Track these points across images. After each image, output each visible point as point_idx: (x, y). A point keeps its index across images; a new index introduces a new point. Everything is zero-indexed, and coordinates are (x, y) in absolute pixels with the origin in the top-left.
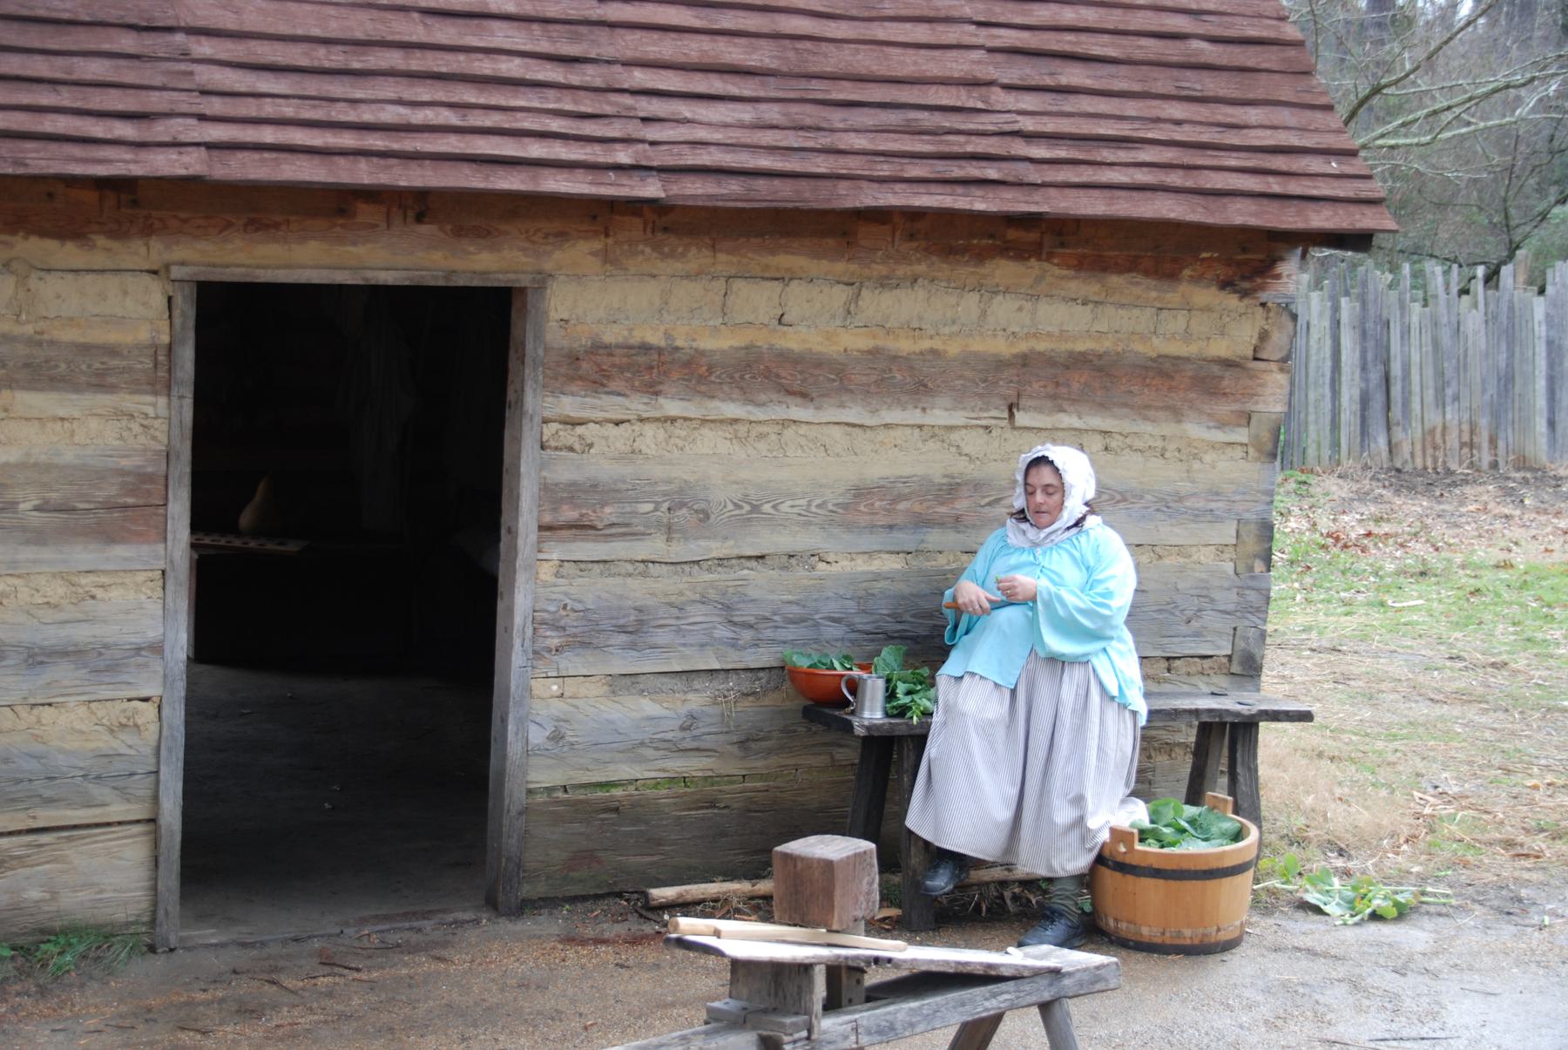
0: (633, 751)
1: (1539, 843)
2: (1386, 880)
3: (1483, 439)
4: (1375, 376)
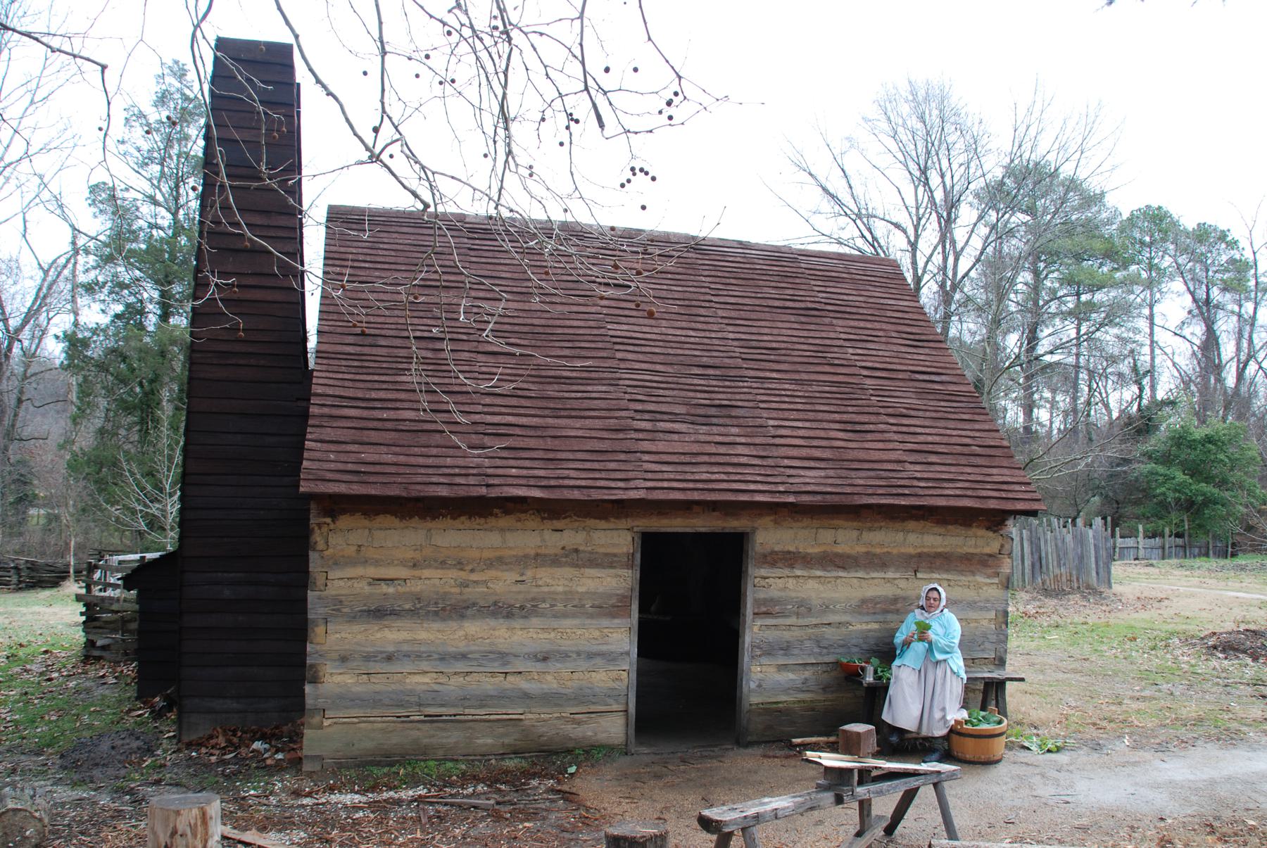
0: (786, 691)
1: (1104, 724)
2: (1052, 738)
3: (1074, 578)
4: (1036, 557)
